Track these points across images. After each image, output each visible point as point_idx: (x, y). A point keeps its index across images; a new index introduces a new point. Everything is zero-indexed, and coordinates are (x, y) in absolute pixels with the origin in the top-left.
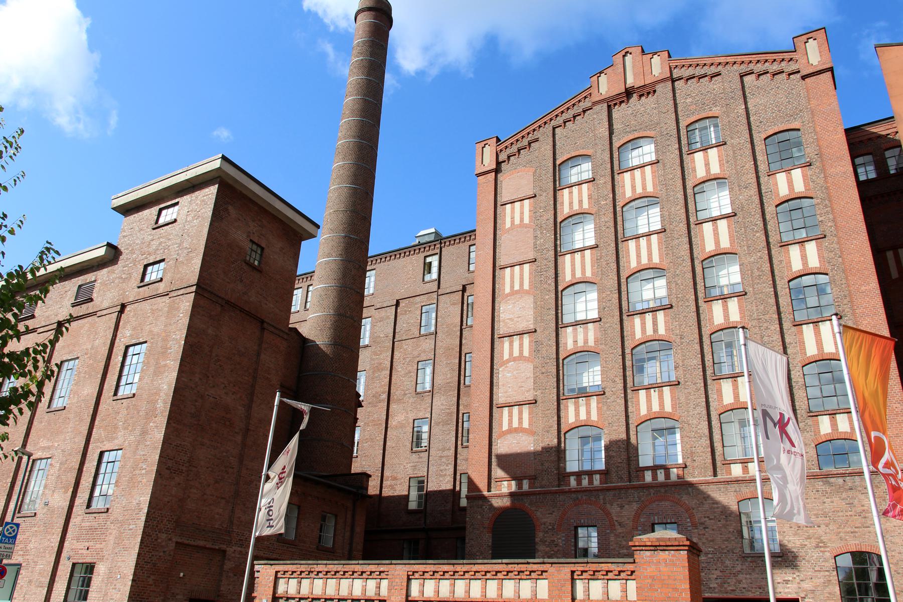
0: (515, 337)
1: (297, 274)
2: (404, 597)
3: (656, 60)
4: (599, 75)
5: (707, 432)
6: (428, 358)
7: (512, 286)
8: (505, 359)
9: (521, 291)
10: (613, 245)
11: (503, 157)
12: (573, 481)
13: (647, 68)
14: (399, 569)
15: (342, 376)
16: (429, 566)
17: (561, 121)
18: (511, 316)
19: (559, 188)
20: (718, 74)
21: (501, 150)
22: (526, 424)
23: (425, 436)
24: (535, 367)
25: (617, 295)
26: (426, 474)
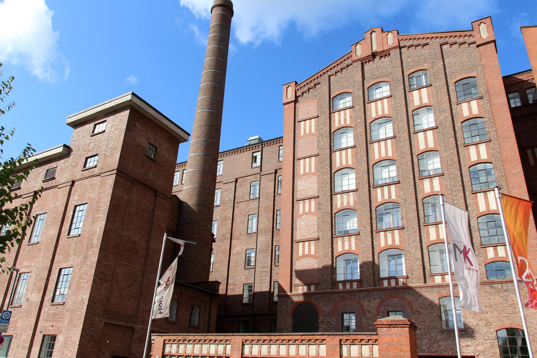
0: (306, 200)
1: (177, 163)
3: (390, 35)
4: (356, 44)
5: (420, 257)
6: (255, 213)
7: (305, 170)
8: (300, 213)
9: (310, 173)
10: (365, 146)
11: (299, 93)
12: (341, 286)
13: (385, 40)
14: (237, 339)
16: (255, 337)
17: (334, 72)
19: (332, 112)
20: (427, 44)
21: (298, 89)
22: (313, 252)
23: (253, 259)
24: (318, 218)
25: (367, 176)
26: (253, 282)
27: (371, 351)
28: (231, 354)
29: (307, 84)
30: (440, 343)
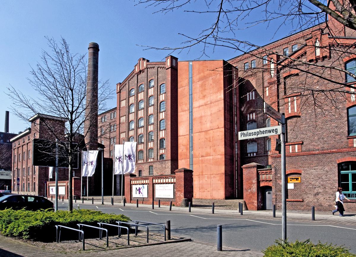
5: (146, 153)
11: (121, 88)
20: (154, 67)
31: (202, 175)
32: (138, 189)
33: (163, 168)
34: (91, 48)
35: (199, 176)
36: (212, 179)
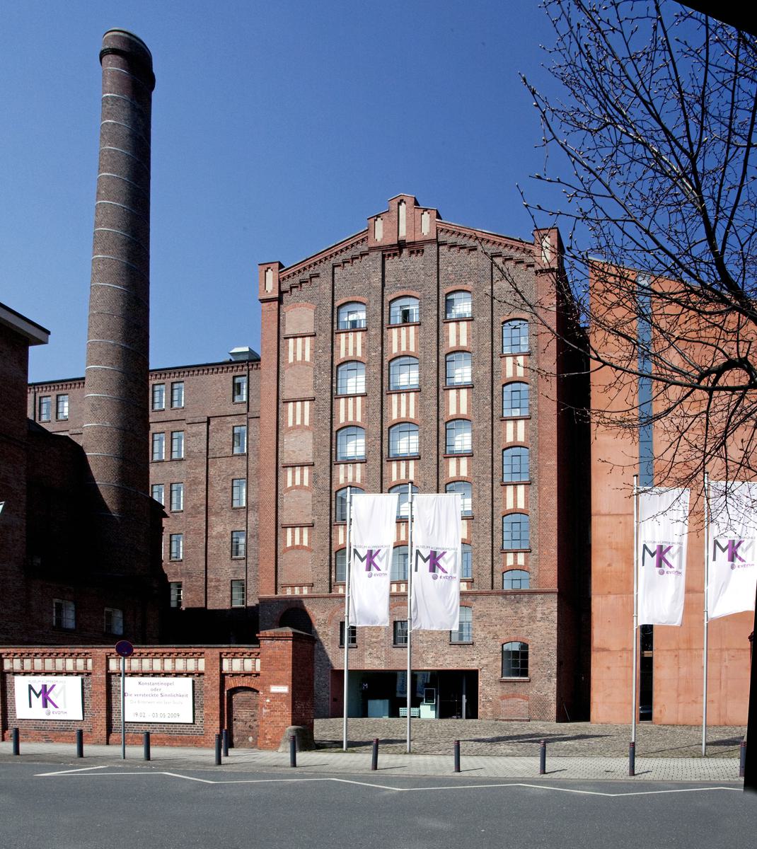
0: (297, 468)
2: (105, 669)
3: (426, 216)
4: (375, 218)
6: (242, 477)
7: (294, 421)
8: (288, 486)
10: (379, 396)
11: (285, 286)
13: (418, 223)
14: (213, 652)
15: (127, 488)
16: (235, 648)
17: (340, 261)
18: (294, 449)
19: (337, 331)
21: (284, 279)
22: (305, 543)
23: (242, 548)
24: (313, 496)
25: (379, 442)
26: (245, 578)
27: (86, 664)
28: (94, 670)
29: (299, 273)
30: (447, 656)
31: (690, 649)
32: (38, 689)
33: (521, 619)
34: (114, 51)
35: (677, 653)
36: (727, 663)
